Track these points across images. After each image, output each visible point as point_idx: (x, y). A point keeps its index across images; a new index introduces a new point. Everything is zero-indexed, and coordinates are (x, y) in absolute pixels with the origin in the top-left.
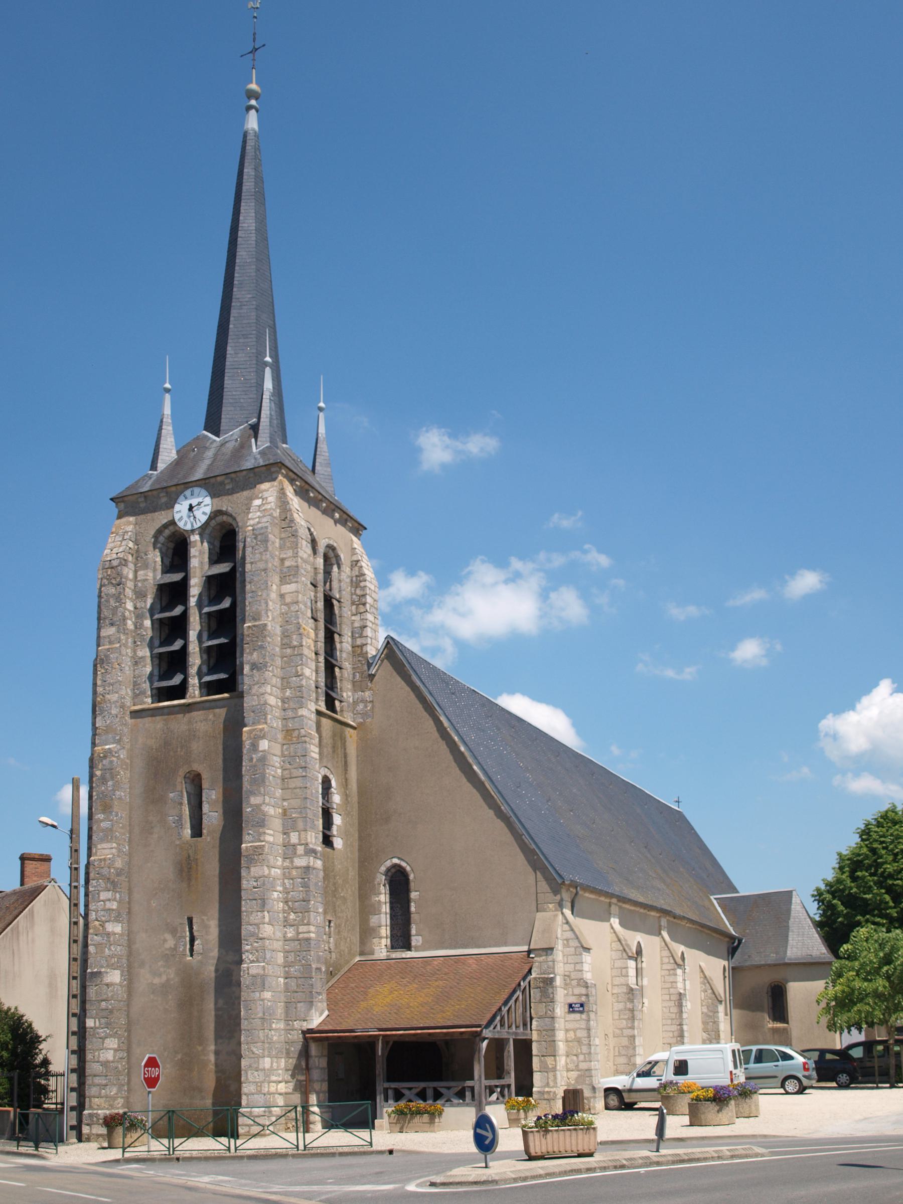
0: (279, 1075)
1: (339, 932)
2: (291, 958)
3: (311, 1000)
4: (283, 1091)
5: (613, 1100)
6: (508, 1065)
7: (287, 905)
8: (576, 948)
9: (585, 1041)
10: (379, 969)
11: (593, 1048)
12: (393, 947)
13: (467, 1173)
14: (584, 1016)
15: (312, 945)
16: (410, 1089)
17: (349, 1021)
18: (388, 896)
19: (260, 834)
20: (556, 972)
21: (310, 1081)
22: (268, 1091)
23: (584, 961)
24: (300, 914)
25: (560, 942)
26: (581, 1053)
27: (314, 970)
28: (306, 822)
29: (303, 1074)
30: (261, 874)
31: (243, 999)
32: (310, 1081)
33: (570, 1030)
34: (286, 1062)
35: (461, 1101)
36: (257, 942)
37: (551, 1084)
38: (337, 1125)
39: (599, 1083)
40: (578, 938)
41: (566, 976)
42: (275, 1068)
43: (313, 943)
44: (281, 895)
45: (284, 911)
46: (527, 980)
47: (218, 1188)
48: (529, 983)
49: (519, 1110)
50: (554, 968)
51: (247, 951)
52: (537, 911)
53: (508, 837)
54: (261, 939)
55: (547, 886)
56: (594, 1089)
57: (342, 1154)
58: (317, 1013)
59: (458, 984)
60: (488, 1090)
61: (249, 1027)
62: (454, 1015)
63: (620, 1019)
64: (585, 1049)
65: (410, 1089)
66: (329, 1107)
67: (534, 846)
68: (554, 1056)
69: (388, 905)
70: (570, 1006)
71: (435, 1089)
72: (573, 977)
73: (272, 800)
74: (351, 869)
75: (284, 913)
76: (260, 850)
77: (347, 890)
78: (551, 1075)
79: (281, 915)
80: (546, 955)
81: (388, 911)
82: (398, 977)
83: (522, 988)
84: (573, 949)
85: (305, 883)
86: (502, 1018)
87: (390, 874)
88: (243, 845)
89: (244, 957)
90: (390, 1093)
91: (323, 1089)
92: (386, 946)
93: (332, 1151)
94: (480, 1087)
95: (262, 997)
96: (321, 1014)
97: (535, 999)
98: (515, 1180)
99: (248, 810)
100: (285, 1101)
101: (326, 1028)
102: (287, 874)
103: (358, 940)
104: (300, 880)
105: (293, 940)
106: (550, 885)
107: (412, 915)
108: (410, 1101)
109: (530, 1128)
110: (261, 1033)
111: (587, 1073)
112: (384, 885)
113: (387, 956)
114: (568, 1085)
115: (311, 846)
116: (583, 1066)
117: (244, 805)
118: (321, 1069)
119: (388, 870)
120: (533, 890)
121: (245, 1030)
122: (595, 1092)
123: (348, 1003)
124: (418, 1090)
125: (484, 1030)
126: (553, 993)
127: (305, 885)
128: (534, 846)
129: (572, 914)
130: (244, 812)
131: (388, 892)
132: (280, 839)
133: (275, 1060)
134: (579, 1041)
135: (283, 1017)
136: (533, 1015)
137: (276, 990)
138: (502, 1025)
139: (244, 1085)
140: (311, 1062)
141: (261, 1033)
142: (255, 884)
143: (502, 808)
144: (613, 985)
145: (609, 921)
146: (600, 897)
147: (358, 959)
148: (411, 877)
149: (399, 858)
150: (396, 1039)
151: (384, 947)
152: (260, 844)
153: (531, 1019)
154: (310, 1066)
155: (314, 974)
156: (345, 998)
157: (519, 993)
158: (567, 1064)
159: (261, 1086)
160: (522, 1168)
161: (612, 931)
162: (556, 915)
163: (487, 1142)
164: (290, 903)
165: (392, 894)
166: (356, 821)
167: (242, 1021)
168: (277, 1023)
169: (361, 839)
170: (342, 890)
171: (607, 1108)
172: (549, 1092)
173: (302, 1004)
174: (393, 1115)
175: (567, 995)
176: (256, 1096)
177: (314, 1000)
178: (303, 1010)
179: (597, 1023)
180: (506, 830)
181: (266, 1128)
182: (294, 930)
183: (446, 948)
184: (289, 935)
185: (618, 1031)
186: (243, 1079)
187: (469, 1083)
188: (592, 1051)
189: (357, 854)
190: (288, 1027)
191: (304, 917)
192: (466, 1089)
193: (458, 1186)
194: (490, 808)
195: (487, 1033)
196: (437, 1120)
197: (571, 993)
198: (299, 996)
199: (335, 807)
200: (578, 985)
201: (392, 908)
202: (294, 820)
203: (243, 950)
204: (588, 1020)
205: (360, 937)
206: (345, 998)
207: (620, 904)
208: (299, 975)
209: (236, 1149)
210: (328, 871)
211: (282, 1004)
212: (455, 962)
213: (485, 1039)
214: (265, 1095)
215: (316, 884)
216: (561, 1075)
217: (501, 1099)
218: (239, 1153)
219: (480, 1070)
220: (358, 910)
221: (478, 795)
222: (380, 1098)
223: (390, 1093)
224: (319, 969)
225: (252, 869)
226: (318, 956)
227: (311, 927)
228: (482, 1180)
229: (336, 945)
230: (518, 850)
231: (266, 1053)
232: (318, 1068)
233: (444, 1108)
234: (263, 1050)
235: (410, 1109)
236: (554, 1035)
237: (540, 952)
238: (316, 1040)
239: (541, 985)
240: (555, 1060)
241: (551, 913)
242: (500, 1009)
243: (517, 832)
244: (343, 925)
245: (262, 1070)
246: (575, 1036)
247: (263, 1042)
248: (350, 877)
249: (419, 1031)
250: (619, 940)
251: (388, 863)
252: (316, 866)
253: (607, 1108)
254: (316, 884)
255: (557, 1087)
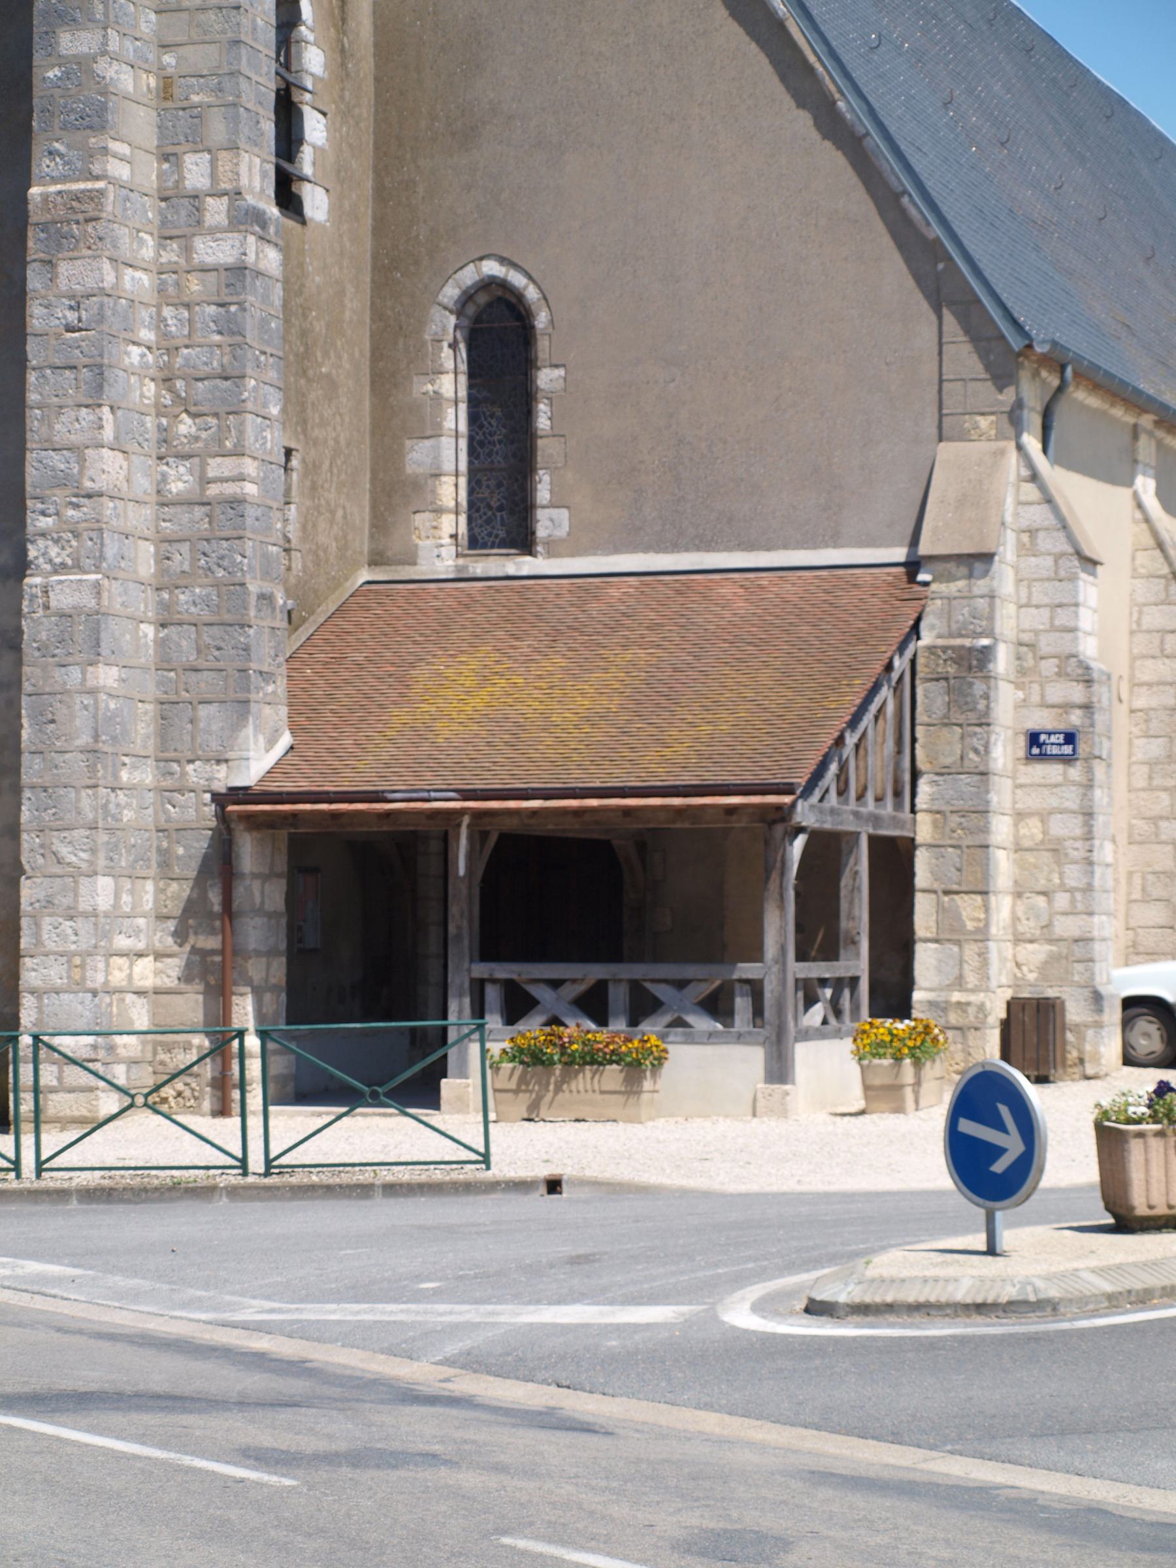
0: (137, 932)
1: (314, 487)
2: (181, 560)
3: (241, 696)
4: (149, 983)
5: (1147, 1035)
6: (851, 917)
7: (171, 390)
8: (1058, 557)
9: (1075, 850)
10: (438, 610)
11: (1098, 871)
12: (476, 542)
13: (931, 1272)
14: (1075, 772)
15: (249, 521)
16: (555, 984)
17: (360, 765)
18: (463, 380)
19: (90, 155)
20: (997, 630)
21: (235, 953)
22: (107, 982)
23: (1081, 599)
24: (213, 421)
25: (1010, 537)
26: (1063, 888)
27: (253, 600)
28: (236, 120)
29: (212, 932)
30: (91, 283)
31: (27, 687)
32: (235, 953)
33: (1031, 814)
34: (159, 891)
35: (719, 1026)
36: (77, 506)
37: (971, 979)
38: (375, 1095)
39: (1109, 982)
40: (1065, 527)
41: (1025, 646)
42: (127, 909)
43: (251, 512)
44: (150, 358)
45: (160, 410)
46: (909, 654)
47: (39, 1303)
48: (913, 662)
49: (898, 1059)
50: (991, 618)
51: (43, 535)
52: (940, 440)
53: (859, 202)
54: (89, 496)
55: (975, 357)
56: (1097, 999)
57: (392, 1189)
58: (261, 738)
59: (697, 657)
60: (800, 994)
61: (47, 780)
62: (699, 754)
63: (1151, 789)
64: (1073, 875)
65: (555, 984)
66: (287, 1035)
67: (937, 231)
68: (984, 893)
69: (463, 407)
70: (1034, 739)
71: (636, 987)
72: (1044, 649)
73: (128, 44)
74: (350, 289)
75: (159, 415)
76: (89, 207)
77: (339, 358)
78: (970, 950)
79: (150, 422)
80: (970, 576)
81: (463, 427)
82: (500, 633)
83: (895, 676)
84: (1049, 562)
85: (231, 318)
86: (843, 767)
87: (471, 310)
88: (35, 191)
89: (32, 553)
90: (493, 994)
91: (273, 981)
92: (454, 536)
93: (365, 1176)
94: (783, 982)
95: (90, 683)
96: (271, 743)
97: (928, 711)
98: (1114, 1301)
99: (50, 74)
100: (154, 1015)
101: (289, 786)
102: (171, 290)
103: (367, 518)
104: (212, 310)
105: (191, 504)
106: (983, 355)
107: (540, 442)
108: (555, 1021)
109: (1130, 1121)
110: (86, 800)
111: (1078, 951)
112: (453, 346)
113: (458, 569)
114: (1016, 986)
115: (250, 200)
116: (1067, 927)
117: (38, 58)
118: (270, 915)
119: (468, 297)
120: (929, 369)
121: (32, 787)
122: (1099, 1010)
123: (352, 711)
124: (581, 988)
125: (800, 804)
126: (986, 697)
127: (231, 328)
128: (937, 231)
129: (1045, 450)
130: (36, 81)
131: (463, 367)
132: (149, 173)
133: (127, 884)
134: (1056, 849)
135: (150, 751)
136: (921, 764)
137: (133, 662)
138: (842, 792)
139: (27, 962)
140: (240, 892)
141: (86, 800)
142: (72, 316)
143: (841, 104)
144: (1135, 684)
145: (1129, 483)
146: (1113, 405)
147: (365, 575)
148: (541, 320)
149: (503, 260)
150: (511, 824)
151: (447, 540)
152: (89, 185)
153: (915, 775)
154: (235, 905)
155: (252, 613)
156: (339, 693)
157: (885, 692)
158: (1015, 919)
159: (82, 966)
160: (1119, 1258)
161: (1138, 515)
162: (1002, 452)
163: (999, 1167)
164: (179, 384)
165: (477, 373)
166: (369, 140)
167: (26, 758)
168: (134, 767)
169: (381, 195)
170: (326, 355)
171: (1128, 1060)
172: (962, 1006)
173: (213, 709)
174: (507, 1066)
175: (1023, 704)
176: (65, 997)
177: (253, 696)
178: (215, 727)
179: (1110, 797)
180: (849, 176)
181: (140, 1100)
182: (190, 472)
183: (646, 549)
184: (176, 488)
185: (1142, 826)
186: (24, 943)
187: (747, 970)
188: (1097, 883)
189: (368, 243)
190: (168, 783)
191: (223, 430)
192: (737, 986)
193: (917, 1318)
194: (801, 105)
195: (806, 814)
196: (647, 1085)
197: (1035, 698)
198: (205, 682)
199: (309, 84)
200: (1061, 674)
201: (474, 419)
202: (198, 115)
203: (30, 529)
204: (1089, 785)
205: (374, 507)
206: (339, 693)
207: (1160, 434)
208: (207, 616)
209: (40, 1168)
210: (293, 280)
211: (149, 707)
212: (679, 592)
213: (800, 830)
214: (95, 993)
215: (263, 323)
216: (1000, 952)
217: (832, 1020)
218: (50, 1181)
219: (783, 929)
220: (368, 421)
221: (764, 61)
222: (458, 1009)
223: (493, 994)
224: (266, 598)
225: (63, 268)
226: (266, 556)
227: (248, 461)
228: (1004, 1299)
229: (304, 528)
230: (887, 241)
231: (102, 862)
232: (260, 911)
233: (670, 1048)
234: (93, 851)
235: (563, 1046)
236: (985, 830)
237: (951, 566)
238: (253, 822)
239: (951, 670)
240: (986, 908)
241: (982, 446)
242: (840, 741)
243: (886, 184)
244: (326, 466)
245: (86, 915)
246: (1045, 833)
247: (94, 828)
248: (348, 314)
249: (594, 802)
250: (1160, 546)
251: (469, 276)
252: (262, 266)
253: (1128, 1060)
254: (263, 323)
255: (987, 990)
